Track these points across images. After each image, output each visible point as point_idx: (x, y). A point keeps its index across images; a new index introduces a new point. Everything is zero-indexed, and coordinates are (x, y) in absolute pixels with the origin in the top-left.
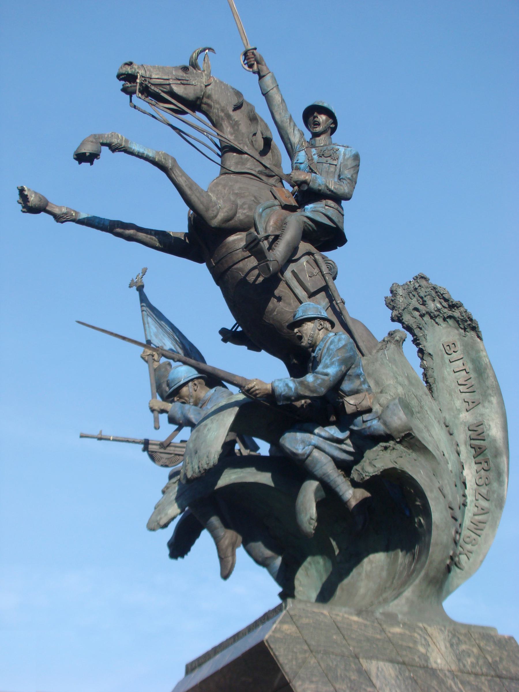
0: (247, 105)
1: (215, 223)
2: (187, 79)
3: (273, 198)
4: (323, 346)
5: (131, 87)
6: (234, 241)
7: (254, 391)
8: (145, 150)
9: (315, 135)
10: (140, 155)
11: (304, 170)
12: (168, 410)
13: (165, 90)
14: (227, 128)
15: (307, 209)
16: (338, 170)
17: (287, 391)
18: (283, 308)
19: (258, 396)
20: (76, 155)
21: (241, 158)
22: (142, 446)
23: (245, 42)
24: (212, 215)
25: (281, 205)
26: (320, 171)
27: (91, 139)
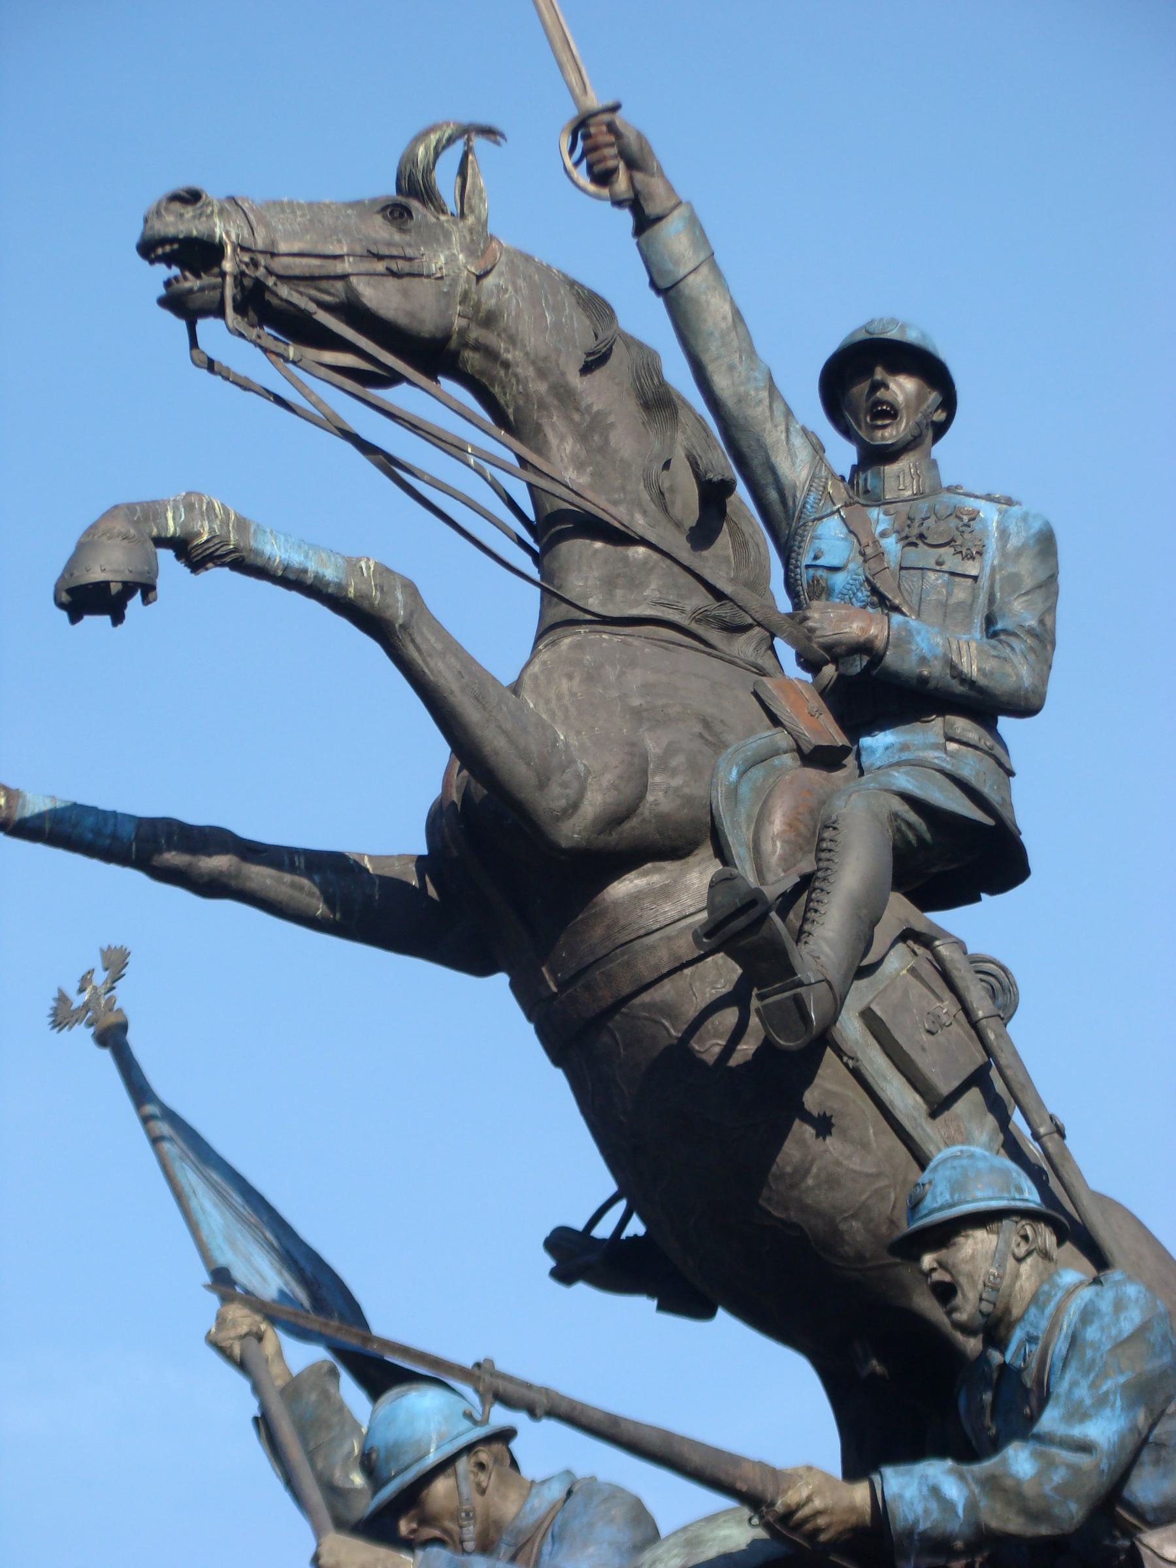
0: (628, 347)
1: (572, 832)
2: (410, 252)
3: (767, 721)
4: (1044, 1324)
5: (202, 289)
6: (637, 897)
7: (806, 1520)
8: (306, 556)
9: (875, 457)
10: (292, 577)
11: (848, 598)
13: (327, 298)
14: (562, 439)
15: (872, 751)
16: (983, 598)
17: (936, 1514)
18: (837, 1164)
20: (70, 591)
21: (625, 560)
23: (574, 79)
24: (563, 802)
25: (799, 750)
26: (915, 599)
27: (120, 526)
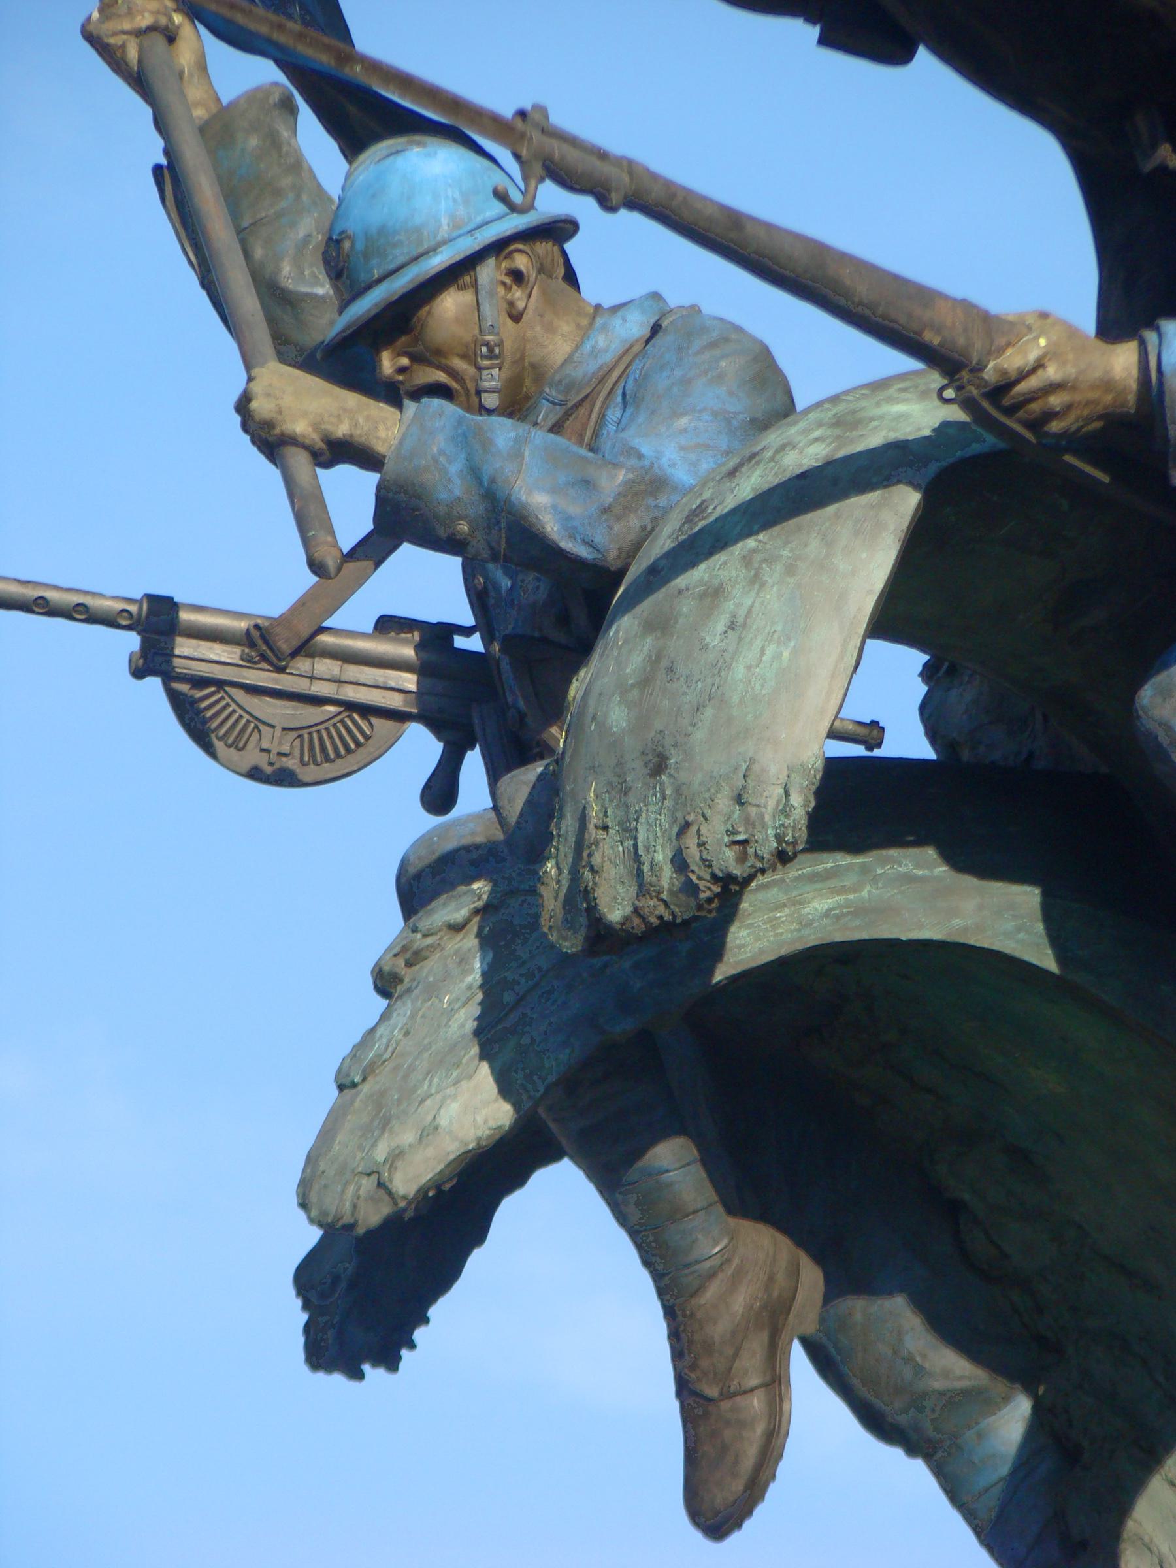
12: (381, 448)
19: (1055, 426)
22: (132, 641)
